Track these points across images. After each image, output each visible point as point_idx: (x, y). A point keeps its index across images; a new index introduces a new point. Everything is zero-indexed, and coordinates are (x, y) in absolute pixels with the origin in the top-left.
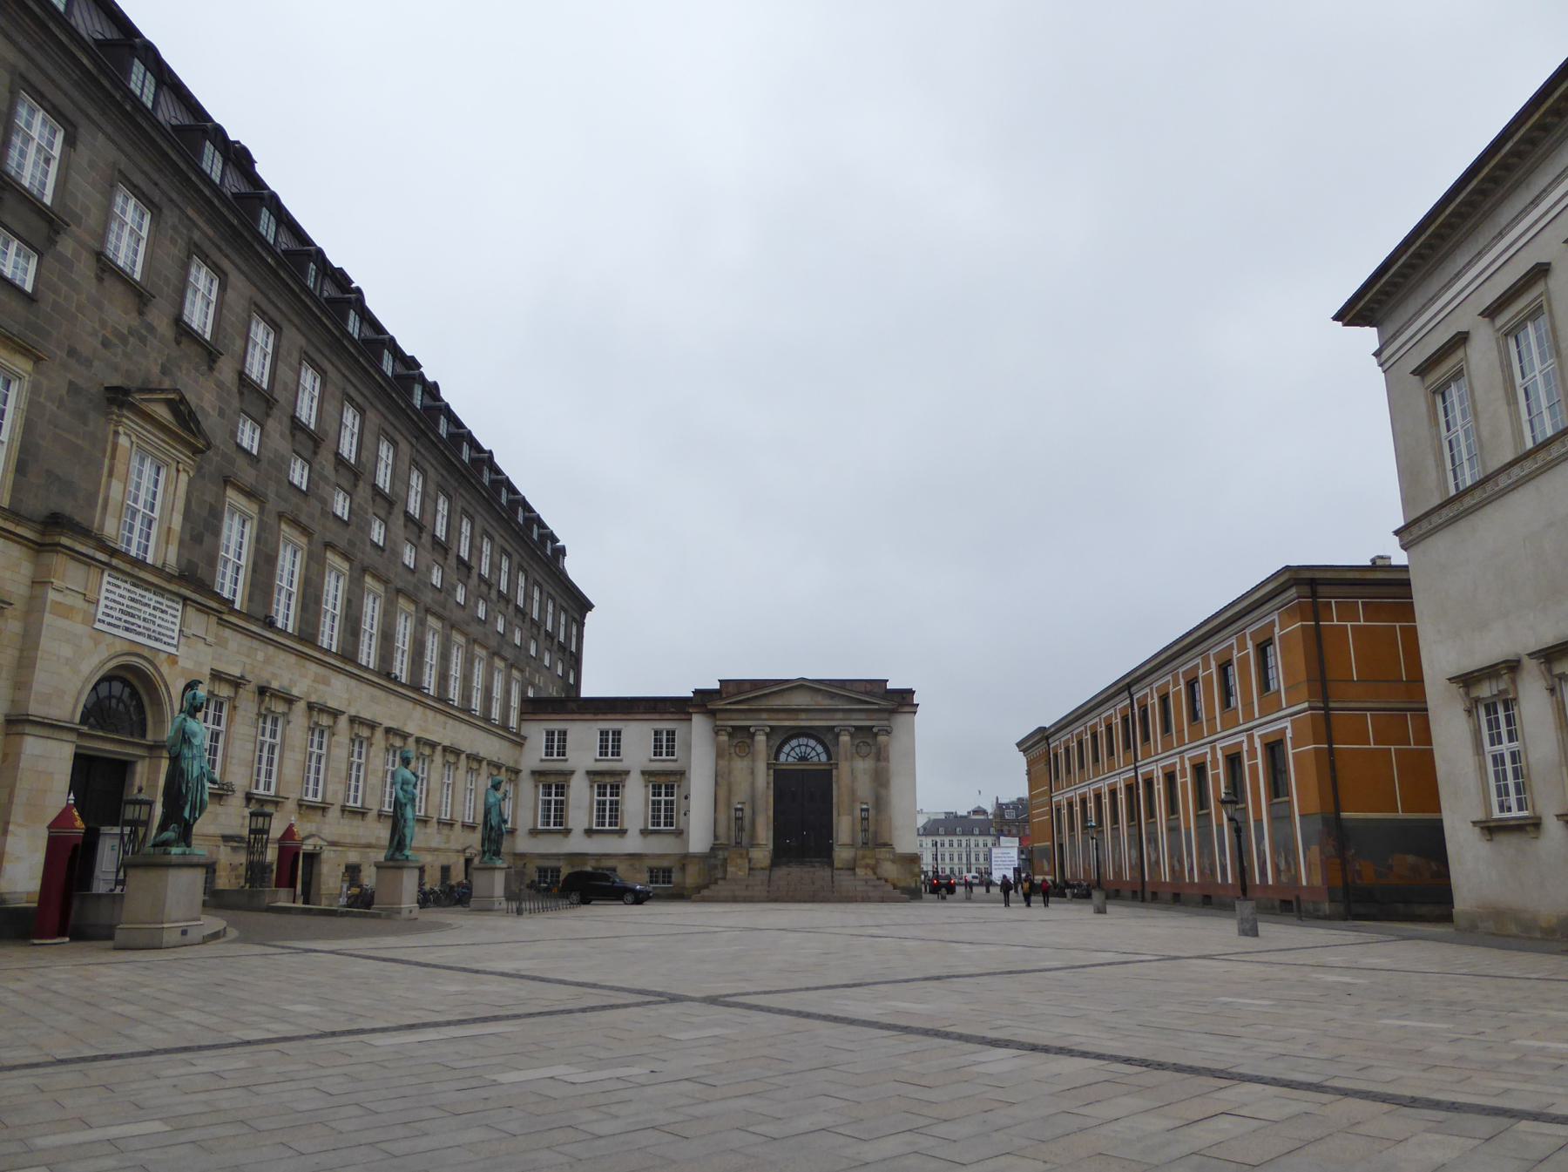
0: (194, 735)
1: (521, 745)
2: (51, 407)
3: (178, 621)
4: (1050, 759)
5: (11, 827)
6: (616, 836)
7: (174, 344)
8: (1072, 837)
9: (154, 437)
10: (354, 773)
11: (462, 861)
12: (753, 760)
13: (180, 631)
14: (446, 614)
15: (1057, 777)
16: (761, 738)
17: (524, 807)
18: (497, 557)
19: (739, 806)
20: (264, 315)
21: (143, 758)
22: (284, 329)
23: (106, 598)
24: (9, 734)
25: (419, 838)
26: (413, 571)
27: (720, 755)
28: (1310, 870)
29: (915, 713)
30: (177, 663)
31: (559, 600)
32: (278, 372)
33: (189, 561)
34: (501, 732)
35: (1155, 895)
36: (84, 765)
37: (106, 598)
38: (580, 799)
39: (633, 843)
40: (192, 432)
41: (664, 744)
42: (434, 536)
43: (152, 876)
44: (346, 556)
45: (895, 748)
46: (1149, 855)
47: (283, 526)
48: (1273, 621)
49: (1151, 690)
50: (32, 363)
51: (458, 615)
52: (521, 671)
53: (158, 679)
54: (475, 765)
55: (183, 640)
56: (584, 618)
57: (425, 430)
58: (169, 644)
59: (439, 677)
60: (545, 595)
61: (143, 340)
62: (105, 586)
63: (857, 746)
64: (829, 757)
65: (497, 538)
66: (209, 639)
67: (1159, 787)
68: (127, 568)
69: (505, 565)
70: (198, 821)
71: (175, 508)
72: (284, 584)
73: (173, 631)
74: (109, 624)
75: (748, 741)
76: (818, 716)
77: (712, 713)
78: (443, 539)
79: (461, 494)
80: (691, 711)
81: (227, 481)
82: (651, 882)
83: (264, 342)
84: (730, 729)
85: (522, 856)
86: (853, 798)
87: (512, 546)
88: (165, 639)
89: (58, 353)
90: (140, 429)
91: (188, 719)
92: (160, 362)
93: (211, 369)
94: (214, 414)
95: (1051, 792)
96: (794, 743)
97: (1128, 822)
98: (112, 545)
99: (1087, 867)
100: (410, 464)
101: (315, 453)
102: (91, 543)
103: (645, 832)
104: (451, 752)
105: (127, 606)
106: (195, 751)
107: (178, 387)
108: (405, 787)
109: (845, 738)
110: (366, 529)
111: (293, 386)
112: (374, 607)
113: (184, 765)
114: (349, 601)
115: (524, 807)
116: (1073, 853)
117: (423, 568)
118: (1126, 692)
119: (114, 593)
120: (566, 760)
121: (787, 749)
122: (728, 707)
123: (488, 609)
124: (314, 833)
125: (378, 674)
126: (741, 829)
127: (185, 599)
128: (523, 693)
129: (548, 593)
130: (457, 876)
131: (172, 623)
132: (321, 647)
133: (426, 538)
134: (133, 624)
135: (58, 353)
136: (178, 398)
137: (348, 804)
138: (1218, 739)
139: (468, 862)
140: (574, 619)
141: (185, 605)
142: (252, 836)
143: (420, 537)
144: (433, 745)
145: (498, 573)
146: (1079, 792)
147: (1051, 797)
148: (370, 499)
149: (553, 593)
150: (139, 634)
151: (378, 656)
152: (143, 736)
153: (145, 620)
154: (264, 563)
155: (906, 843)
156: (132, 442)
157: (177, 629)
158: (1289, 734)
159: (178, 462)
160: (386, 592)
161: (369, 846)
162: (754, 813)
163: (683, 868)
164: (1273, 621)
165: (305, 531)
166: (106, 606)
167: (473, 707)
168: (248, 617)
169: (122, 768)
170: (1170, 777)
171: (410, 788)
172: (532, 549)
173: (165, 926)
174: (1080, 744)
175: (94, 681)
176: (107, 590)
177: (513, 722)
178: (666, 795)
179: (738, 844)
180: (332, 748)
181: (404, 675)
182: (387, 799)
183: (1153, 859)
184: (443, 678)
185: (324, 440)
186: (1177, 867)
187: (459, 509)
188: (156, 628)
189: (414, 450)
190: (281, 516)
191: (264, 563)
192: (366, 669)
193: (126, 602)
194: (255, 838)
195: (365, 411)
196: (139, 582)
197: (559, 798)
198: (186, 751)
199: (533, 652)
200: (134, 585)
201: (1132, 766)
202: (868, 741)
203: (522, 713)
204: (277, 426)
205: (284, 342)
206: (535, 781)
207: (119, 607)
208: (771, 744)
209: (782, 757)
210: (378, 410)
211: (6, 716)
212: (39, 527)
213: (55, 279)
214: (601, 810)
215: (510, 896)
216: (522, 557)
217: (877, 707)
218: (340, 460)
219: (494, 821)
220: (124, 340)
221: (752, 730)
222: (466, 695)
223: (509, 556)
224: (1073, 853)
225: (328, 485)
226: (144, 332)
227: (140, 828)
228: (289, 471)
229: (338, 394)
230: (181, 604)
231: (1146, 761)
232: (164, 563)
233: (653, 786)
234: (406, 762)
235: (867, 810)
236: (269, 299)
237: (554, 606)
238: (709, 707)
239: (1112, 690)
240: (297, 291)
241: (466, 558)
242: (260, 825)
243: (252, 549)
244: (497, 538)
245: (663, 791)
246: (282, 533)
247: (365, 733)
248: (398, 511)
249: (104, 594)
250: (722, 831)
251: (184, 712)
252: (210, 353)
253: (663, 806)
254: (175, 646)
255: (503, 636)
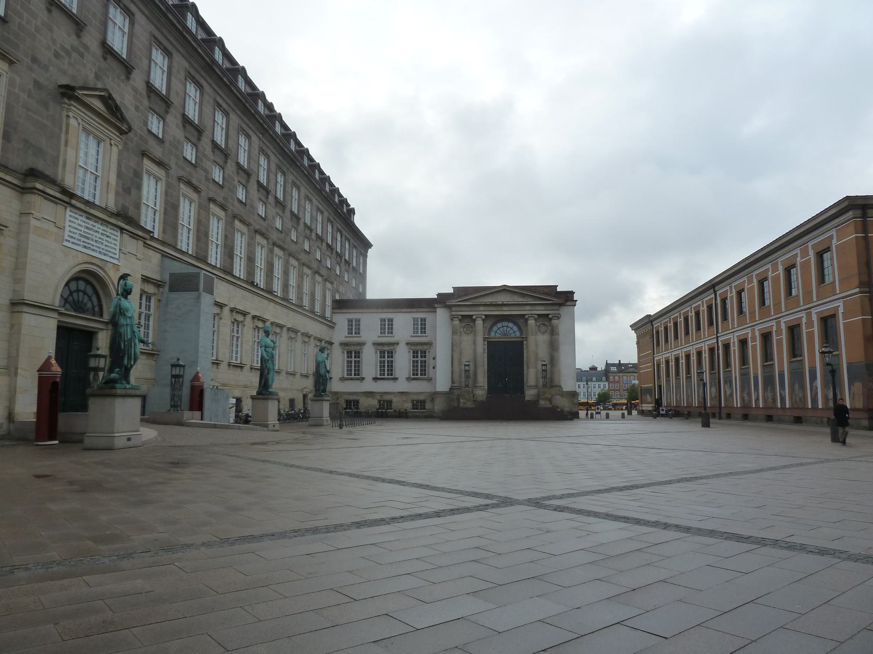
0: (127, 310)
1: (333, 328)
2: (23, 96)
3: (118, 244)
4: (653, 334)
5: (19, 371)
6: (392, 381)
7: (102, 60)
8: (668, 381)
9: (95, 122)
10: (235, 343)
11: (301, 396)
12: (475, 336)
13: (120, 249)
14: (286, 246)
15: (658, 344)
16: (479, 322)
17: (337, 364)
18: (314, 213)
19: (467, 363)
20: (159, 44)
21: (102, 329)
22: (174, 56)
23: (70, 226)
24: (13, 312)
25: (278, 384)
26: (264, 219)
27: (454, 332)
28: (854, 398)
29: (575, 305)
30: (119, 270)
31: (352, 241)
32: (172, 84)
33: (124, 206)
34: (321, 320)
35: (729, 416)
36: (64, 332)
37: (70, 226)
38: (370, 360)
39: (402, 385)
40: (118, 119)
41: (421, 326)
42: (276, 198)
43: (108, 400)
44: (223, 207)
45: (562, 325)
46: (725, 392)
47: (182, 186)
48: (832, 236)
49: (731, 288)
50: (7, 65)
51: (293, 248)
52: (332, 283)
53: (110, 283)
54: (306, 340)
55: (122, 255)
56: (367, 252)
57: (268, 129)
58: (113, 258)
59: (283, 286)
60: (344, 237)
61: (82, 55)
62: (68, 218)
63: (539, 326)
64: (521, 334)
65: (314, 201)
66: (139, 256)
67: (735, 349)
68: (82, 206)
69: (320, 218)
70: (134, 367)
71: (111, 169)
72: (185, 223)
73: (115, 249)
74: (73, 243)
75: (471, 324)
76: (515, 308)
77: (449, 307)
78: (282, 200)
79: (291, 172)
80: (436, 306)
81: (144, 154)
82: (413, 409)
83: (162, 63)
84: (460, 317)
85: (336, 393)
86: (537, 359)
87: (323, 207)
88: (111, 254)
89: (25, 59)
90: (83, 115)
91: (123, 299)
92: (94, 70)
93: (128, 78)
94: (132, 109)
95: (654, 354)
96: (499, 325)
97: (666, 378)
98: (72, 191)
99: (679, 399)
100: (259, 151)
101: (199, 140)
102: (56, 188)
103: (409, 379)
104: (292, 331)
105: (84, 232)
106: (128, 321)
107: (107, 88)
108: (267, 349)
109: (531, 322)
110: (233, 190)
111: (182, 94)
112: (241, 241)
113: (122, 330)
114: (226, 236)
115: (337, 364)
116: (668, 389)
117: (270, 217)
118: (712, 290)
119: (75, 223)
120: (360, 337)
121: (495, 328)
122: (459, 303)
123: (311, 245)
124: (209, 378)
125: (247, 282)
126: (468, 377)
127: (122, 229)
128: (333, 296)
129: (346, 237)
130: (299, 406)
131: (114, 244)
132: (211, 265)
133: (271, 199)
134: (89, 244)
135: (25, 59)
136: (107, 95)
137: (232, 361)
138: (756, 325)
139: (305, 396)
140: (361, 254)
141: (122, 233)
142: (173, 380)
143: (267, 198)
144: (281, 327)
145: (315, 222)
146: (674, 353)
147: (654, 357)
148: (236, 171)
149: (348, 236)
150: (94, 250)
151: (245, 270)
152: (101, 315)
153: (96, 241)
154: (171, 210)
155: (568, 384)
156: (79, 123)
157: (118, 248)
158: (841, 310)
159: (111, 139)
160: (249, 231)
161: (245, 387)
162: (475, 367)
163: (433, 400)
164: (832, 236)
165: (196, 189)
166: (70, 231)
167: (304, 304)
168: (163, 243)
169: (89, 336)
170: (743, 343)
171: (270, 350)
172: (335, 208)
173: (116, 435)
174: (676, 324)
175: (66, 280)
176: (70, 221)
177: (328, 314)
178: (421, 358)
179: (467, 386)
180: (220, 327)
181: (262, 283)
182: (255, 359)
183: (728, 393)
184: (286, 286)
185: (204, 132)
186: (746, 398)
187: (290, 181)
188: (103, 247)
189: (261, 142)
190: (180, 179)
191: (171, 210)
192: (239, 279)
193: (83, 229)
194: (175, 380)
195: (229, 114)
196: (90, 216)
197: (357, 359)
198: (122, 321)
199: (338, 272)
200: (87, 218)
201: (715, 336)
202: (546, 323)
203: (333, 308)
204: (173, 119)
205: (175, 64)
206: (342, 348)
207: (78, 232)
208: (485, 326)
209: (493, 334)
210: (236, 113)
211: (11, 300)
212: (22, 177)
213: (19, 8)
214: (382, 366)
215: (333, 417)
216: (329, 213)
217: (551, 302)
218: (215, 146)
219: (322, 371)
220: (68, 54)
221: (474, 317)
222: (300, 298)
223: (322, 213)
224: (668, 389)
225: (209, 161)
226: (82, 50)
227: (99, 373)
228: (183, 150)
229: (212, 101)
230: (119, 232)
231: (698, 342)
232: (107, 203)
233: (413, 351)
234: (267, 333)
235: (545, 365)
236: (163, 34)
237: (349, 244)
238: (447, 304)
239: (696, 293)
240: (181, 29)
241: (296, 213)
242: (178, 373)
243: (163, 200)
244: (314, 201)
245: (386, 355)
246: (181, 190)
247: (240, 318)
248: (253, 181)
249: (68, 223)
250: (456, 377)
251: (119, 295)
252: (127, 67)
253: (419, 364)
254: (117, 259)
255: (320, 261)
